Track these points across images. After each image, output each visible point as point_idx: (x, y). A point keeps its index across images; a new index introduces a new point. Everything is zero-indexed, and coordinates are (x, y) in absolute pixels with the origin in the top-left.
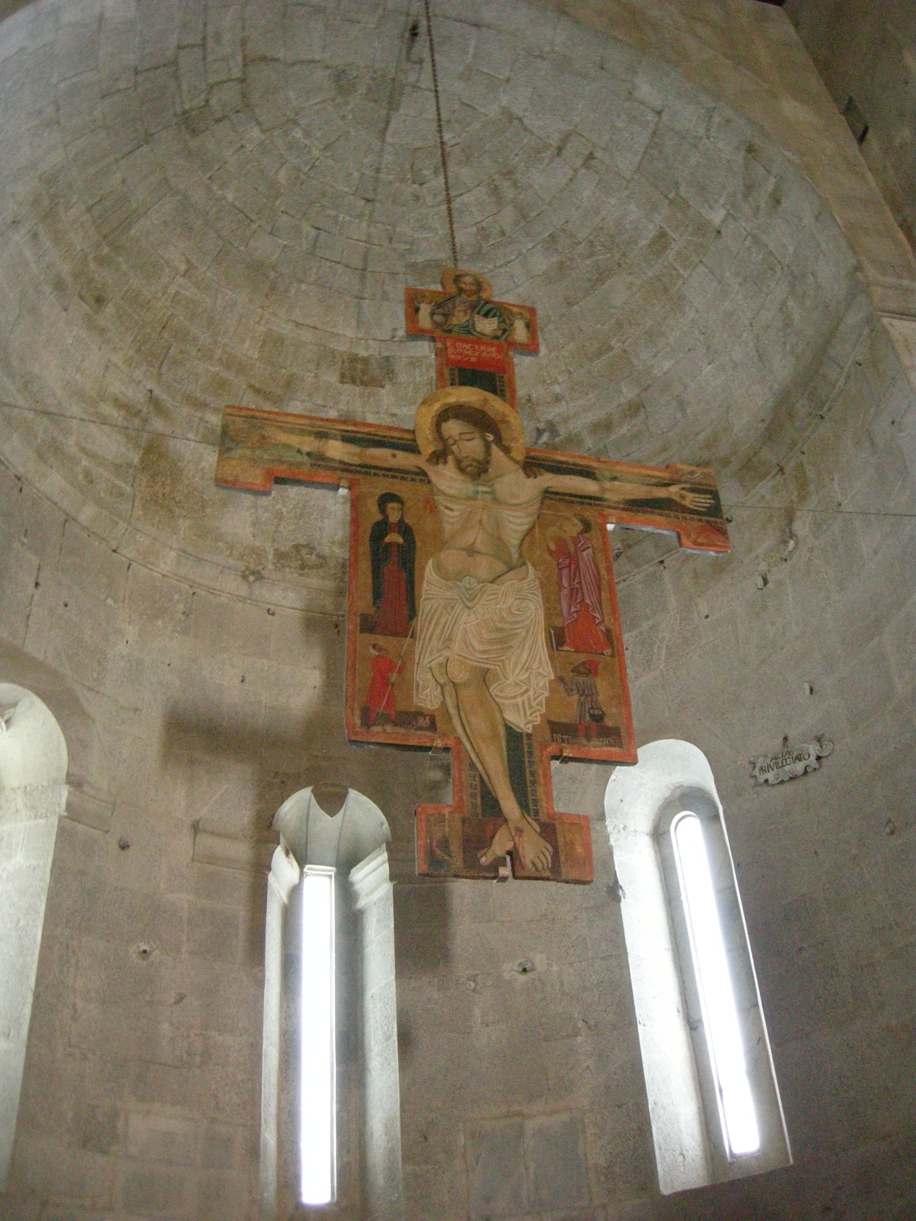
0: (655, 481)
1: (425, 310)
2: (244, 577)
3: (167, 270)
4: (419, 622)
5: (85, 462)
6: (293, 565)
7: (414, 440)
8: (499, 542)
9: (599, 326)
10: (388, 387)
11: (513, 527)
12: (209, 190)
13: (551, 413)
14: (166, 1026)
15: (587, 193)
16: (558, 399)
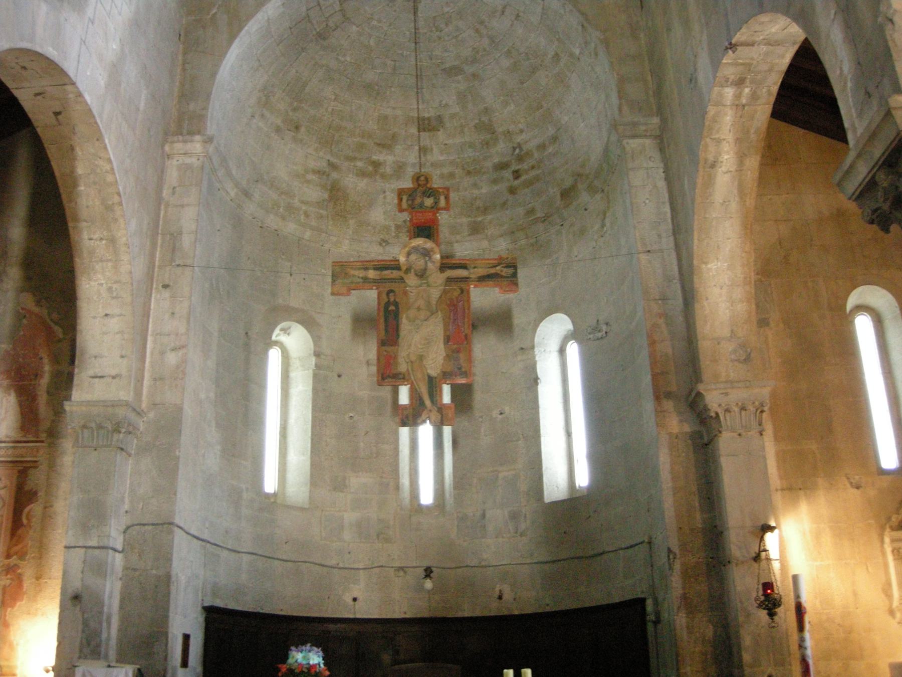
0: (491, 265)
1: (405, 198)
2: (381, 244)
3: (325, 101)
4: (400, 340)
5: (304, 208)
6: (403, 231)
7: (399, 264)
8: (429, 303)
9: (536, 95)
10: (442, 130)
11: (434, 296)
12: (337, 59)
13: (519, 139)
14: (362, 444)
15: (520, 31)
16: (522, 131)
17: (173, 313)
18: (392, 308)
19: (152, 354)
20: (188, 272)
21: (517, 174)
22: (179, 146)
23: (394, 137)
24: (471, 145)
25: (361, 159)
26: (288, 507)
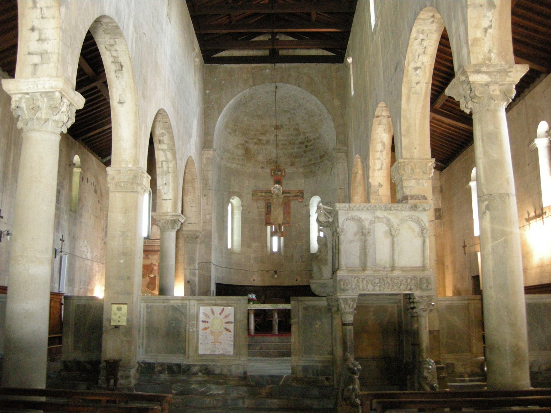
1: (273, 172)
2: (262, 168)
13: (307, 135)
16: (308, 133)
17: (207, 204)
18: (269, 204)
19: (202, 215)
20: (211, 191)
21: (306, 147)
22: (206, 152)
23: (266, 131)
24: (292, 135)
25: (255, 139)
26: (235, 253)
